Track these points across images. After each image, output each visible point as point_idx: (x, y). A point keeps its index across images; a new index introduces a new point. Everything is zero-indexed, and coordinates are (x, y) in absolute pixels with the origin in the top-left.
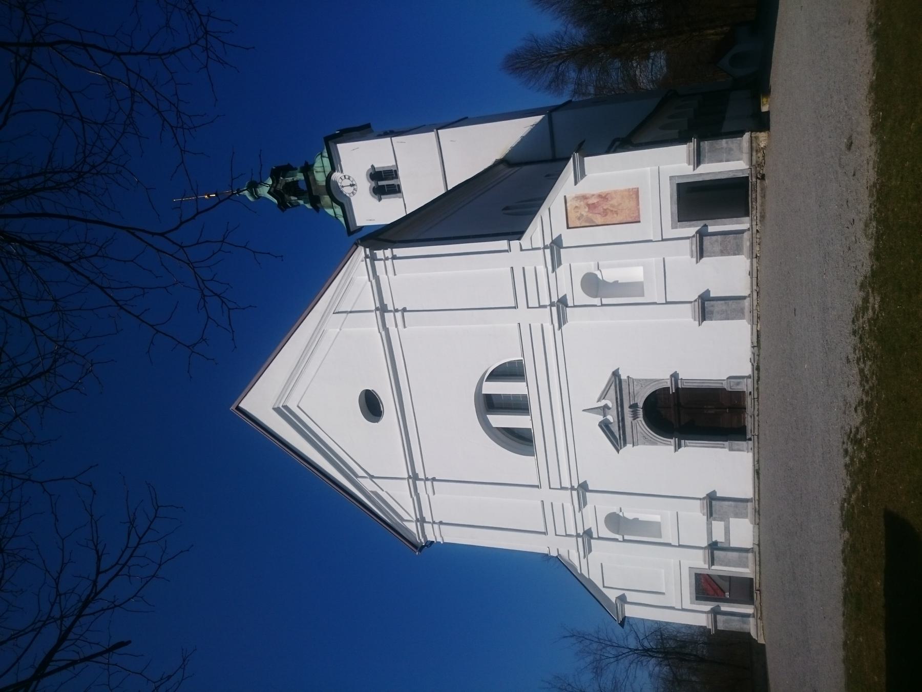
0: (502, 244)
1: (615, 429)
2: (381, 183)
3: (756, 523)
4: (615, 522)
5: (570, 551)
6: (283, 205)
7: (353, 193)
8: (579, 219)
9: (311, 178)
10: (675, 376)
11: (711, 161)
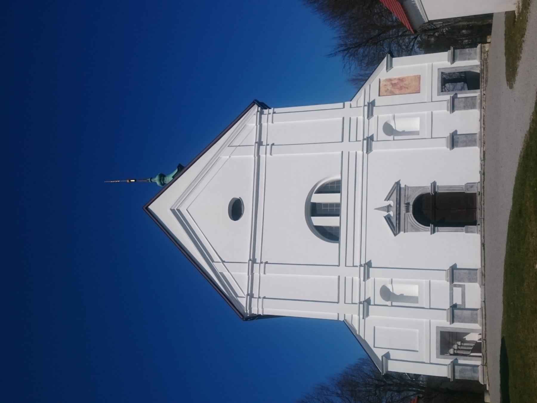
0: (340, 105)
1: (394, 220)
3: (483, 284)
8: (386, 91)
10: (434, 184)
11: (460, 60)
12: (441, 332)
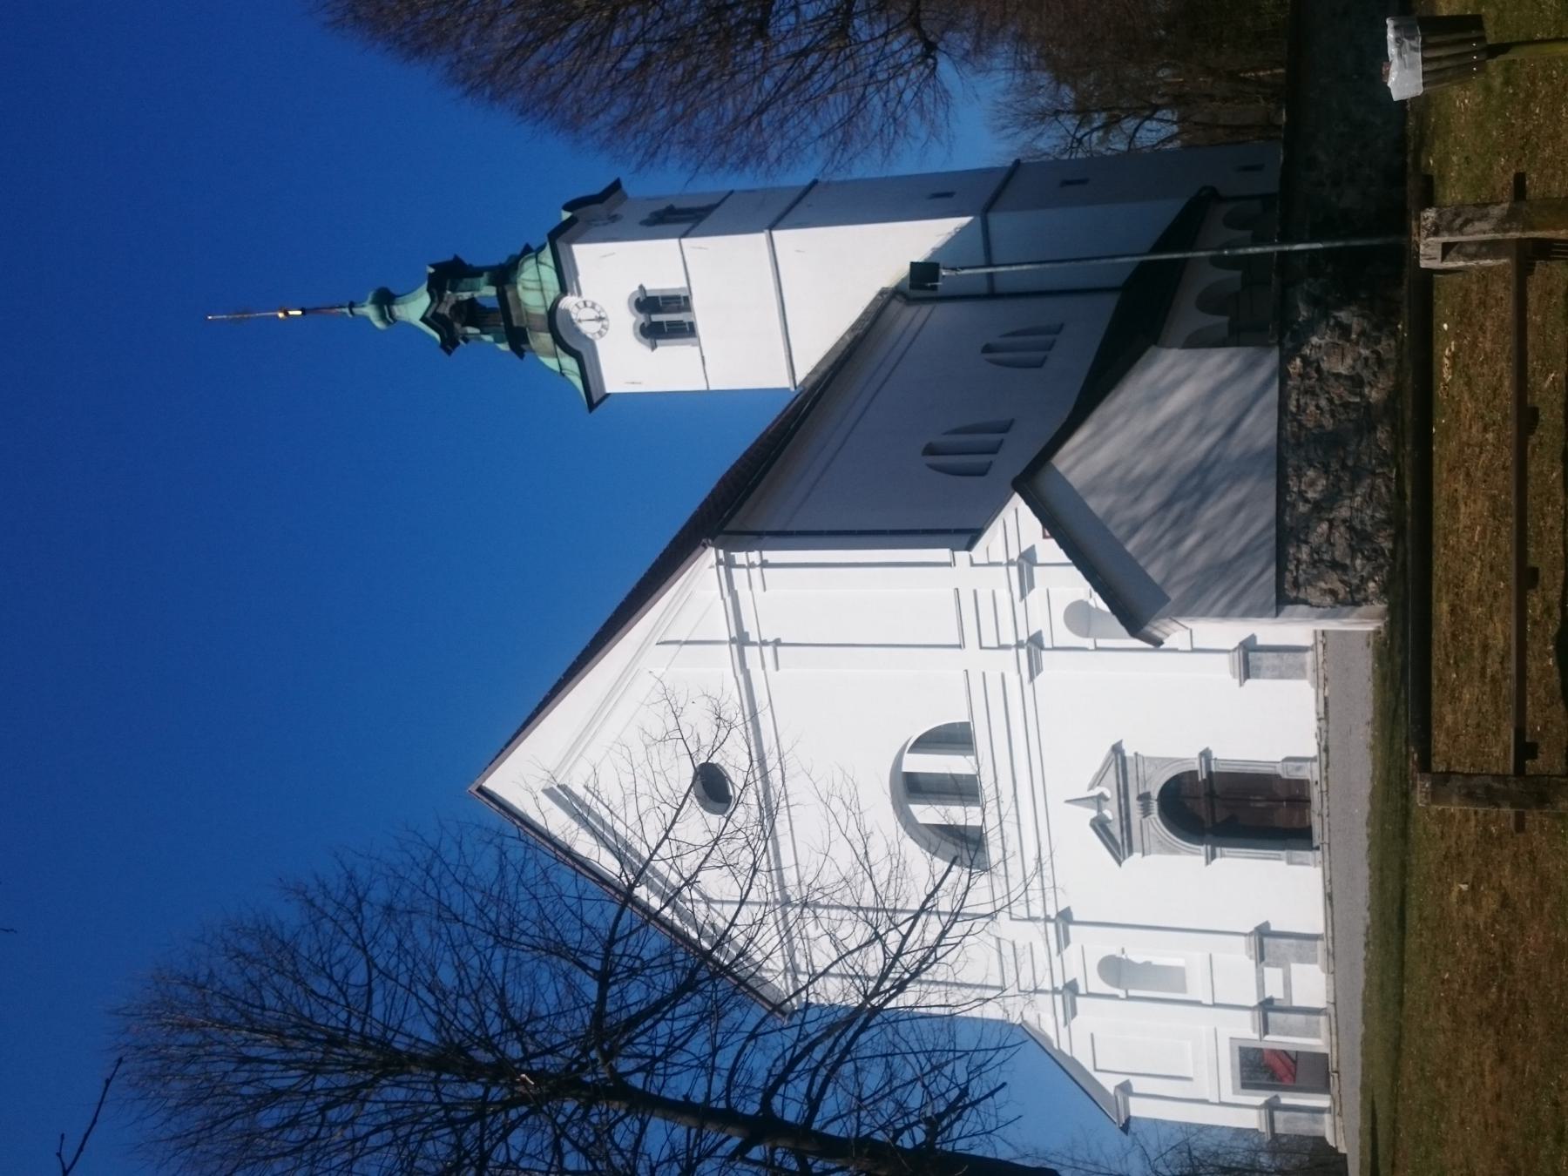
0: (943, 554)
1: (1115, 829)
2: (656, 318)
4: (1115, 969)
5: (1044, 1017)
6: (450, 343)
7: (600, 332)
9: (509, 294)
10: (1206, 755)
12: (1241, 1049)
